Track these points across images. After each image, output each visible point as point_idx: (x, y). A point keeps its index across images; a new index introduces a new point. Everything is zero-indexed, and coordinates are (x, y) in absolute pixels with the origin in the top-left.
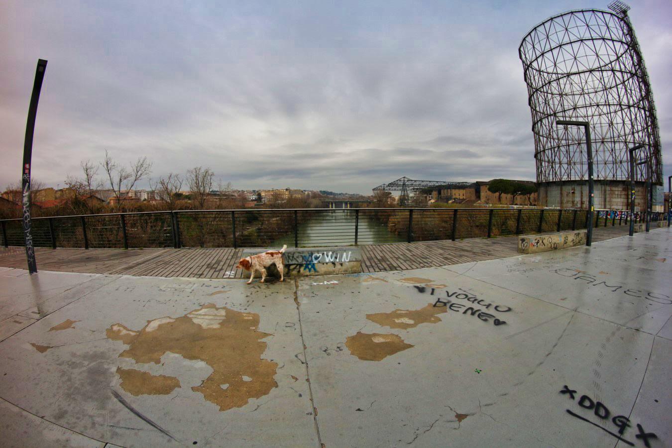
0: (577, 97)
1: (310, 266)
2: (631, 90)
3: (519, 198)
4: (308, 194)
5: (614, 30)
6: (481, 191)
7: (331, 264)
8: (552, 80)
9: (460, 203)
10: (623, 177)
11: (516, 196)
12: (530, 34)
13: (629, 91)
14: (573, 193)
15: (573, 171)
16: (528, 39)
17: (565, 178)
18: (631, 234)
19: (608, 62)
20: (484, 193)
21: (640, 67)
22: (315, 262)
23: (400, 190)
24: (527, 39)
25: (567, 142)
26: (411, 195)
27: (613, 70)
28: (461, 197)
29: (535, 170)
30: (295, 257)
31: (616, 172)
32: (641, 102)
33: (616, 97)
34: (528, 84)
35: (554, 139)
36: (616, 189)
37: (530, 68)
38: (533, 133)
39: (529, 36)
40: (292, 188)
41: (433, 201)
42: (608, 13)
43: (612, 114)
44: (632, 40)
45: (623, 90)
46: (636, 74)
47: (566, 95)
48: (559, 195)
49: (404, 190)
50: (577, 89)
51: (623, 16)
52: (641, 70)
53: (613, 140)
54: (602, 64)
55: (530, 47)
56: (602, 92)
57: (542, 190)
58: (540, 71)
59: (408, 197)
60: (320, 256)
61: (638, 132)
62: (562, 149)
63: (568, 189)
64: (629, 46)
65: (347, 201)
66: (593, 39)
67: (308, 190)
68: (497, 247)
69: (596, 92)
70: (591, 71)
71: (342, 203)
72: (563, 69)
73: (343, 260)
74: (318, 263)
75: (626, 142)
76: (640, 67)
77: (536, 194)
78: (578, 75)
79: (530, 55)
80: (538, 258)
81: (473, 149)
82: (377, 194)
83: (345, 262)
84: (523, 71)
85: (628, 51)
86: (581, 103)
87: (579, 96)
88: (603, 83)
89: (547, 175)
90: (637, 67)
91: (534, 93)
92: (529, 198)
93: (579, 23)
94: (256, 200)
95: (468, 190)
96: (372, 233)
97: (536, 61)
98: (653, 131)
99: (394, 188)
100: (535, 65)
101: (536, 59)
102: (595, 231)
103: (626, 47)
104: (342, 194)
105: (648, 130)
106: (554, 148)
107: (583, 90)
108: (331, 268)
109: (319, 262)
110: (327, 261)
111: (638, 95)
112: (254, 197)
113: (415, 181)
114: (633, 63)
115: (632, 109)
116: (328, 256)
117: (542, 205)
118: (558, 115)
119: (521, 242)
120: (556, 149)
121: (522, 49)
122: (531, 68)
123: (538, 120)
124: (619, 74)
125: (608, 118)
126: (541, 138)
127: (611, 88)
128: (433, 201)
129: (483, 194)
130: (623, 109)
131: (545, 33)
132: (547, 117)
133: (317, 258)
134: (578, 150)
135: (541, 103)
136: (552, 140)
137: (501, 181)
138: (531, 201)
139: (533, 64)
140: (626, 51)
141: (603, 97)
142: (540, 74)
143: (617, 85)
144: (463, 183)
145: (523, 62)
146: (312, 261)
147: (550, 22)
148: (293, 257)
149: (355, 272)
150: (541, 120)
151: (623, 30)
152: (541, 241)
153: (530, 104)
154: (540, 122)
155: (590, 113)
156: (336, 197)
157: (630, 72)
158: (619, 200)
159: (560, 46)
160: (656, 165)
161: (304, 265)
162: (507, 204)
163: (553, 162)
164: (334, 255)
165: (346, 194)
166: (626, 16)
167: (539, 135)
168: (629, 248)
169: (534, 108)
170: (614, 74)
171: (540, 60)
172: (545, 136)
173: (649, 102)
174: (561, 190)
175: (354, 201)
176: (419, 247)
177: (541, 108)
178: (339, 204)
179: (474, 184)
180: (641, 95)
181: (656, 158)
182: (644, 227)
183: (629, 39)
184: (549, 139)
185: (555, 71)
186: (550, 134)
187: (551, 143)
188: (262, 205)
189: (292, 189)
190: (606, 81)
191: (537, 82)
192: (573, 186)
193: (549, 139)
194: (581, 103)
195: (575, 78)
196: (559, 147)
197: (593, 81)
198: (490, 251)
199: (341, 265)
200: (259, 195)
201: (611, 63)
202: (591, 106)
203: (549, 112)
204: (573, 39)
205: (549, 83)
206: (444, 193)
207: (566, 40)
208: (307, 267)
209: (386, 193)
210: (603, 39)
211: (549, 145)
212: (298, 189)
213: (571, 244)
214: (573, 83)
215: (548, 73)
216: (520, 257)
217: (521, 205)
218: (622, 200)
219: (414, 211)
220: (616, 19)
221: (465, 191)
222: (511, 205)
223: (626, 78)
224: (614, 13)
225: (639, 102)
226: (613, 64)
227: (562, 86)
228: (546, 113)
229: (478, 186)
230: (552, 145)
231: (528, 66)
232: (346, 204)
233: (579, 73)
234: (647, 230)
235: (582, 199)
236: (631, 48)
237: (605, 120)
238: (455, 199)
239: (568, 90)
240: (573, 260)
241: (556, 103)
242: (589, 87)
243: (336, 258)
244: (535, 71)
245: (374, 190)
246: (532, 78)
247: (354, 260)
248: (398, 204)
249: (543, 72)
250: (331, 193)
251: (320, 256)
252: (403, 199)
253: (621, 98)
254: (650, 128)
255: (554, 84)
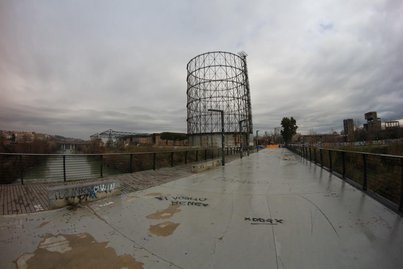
0: (212, 92)
1: (93, 195)
2: (240, 91)
3: (177, 142)
4: (48, 137)
5: (238, 64)
6: (156, 139)
7: (104, 192)
8: (201, 82)
9: (144, 146)
10: (233, 130)
11: (176, 141)
12: (195, 58)
13: (239, 91)
14: (208, 139)
15: (207, 128)
16: (194, 60)
17: (203, 132)
18: (241, 158)
19: (231, 77)
20: (158, 140)
21: (246, 81)
22: (96, 192)
23: (107, 137)
24: (193, 60)
25: (205, 113)
26: (114, 141)
27: (233, 82)
28: (144, 142)
29: (186, 127)
30: (83, 190)
31: (230, 128)
32: (244, 97)
33: (232, 93)
34: (188, 83)
35: (198, 112)
36: (230, 136)
37: (191, 75)
38: (187, 108)
39: (195, 59)
40: (37, 132)
41: (127, 145)
42: (237, 56)
43: (229, 101)
44: (245, 69)
45: (236, 91)
46: (244, 84)
47: (207, 90)
48: (200, 140)
49: (110, 137)
50: (213, 88)
51: (243, 58)
52: (247, 83)
53: (228, 114)
54: (228, 78)
55: (194, 64)
56: (226, 91)
57: (190, 138)
58: (196, 77)
59: (112, 142)
60: (98, 188)
61: (241, 110)
62: (202, 117)
63: (204, 137)
64: (243, 72)
65: (73, 143)
66: (226, 66)
67: (47, 134)
68: (178, 172)
69: (223, 90)
70: (222, 80)
71: (69, 145)
72: (208, 77)
73: (111, 189)
74: (97, 193)
75: (235, 115)
76: (246, 81)
77: (187, 140)
78: (215, 82)
79: (193, 68)
80: (203, 175)
81: (151, 115)
82: (93, 139)
83: (112, 189)
84: (187, 75)
85: (242, 74)
86: (214, 95)
87: (214, 91)
88: (227, 87)
89: (193, 131)
90: (245, 81)
91: (190, 88)
92: (183, 142)
93: (222, 57)
94: (11, 139)
95: (148, 138)
96: (90, 167)
97: (195, 72)
98: (249, 110)
99: (103, 136)
100: (194, 73)
101: (195, 71)
102: (226, 158)
103: (241, 72)
104: (69, 138)
105: (246, 110)
106: (197, 116)
107: (216, 88)
108: (105, 194)
109: (98, 192)
110: (102, 190)
111: (243, 94)
112: (9, 137)
113: (117, 132)
114: (243, 79)
115: (239, 99)
116: (102, 187)
117: (191, 146)
118: (201, 100)
119: (193, 168)
120: (199, 117)
121: (189, 65)
122: (192, 75)
123: (191, 101)
124: (235, 84)
125: (227, 103)
126: (191, 111)
127: (230, 89)
128: (127, 145)
129: (157, 141)
130: (235, 99)
131: (203, 59)
132: (196, 101)
133: (96, 189)
134: (210, 118)
135: (193, 93)
136: (197, 112)
137: (168, 133)
138: (184, 144)
139: (193, 73)
140: (241, 74)
141: (226, 93)
142: (196, 79)
143: (233, 88)
144: (145, 134)
145: (188, 71)
146: (93, 191)
147: (207, 54)
148: (82, 190)
149: (117, 195)
150: (192, 102)
151: (242, 64)
152: (202, 167)
153: (187, 93)
154: (191, 103)
155: (218, 100)
156: (66, 140)
157: (241, 83)
158: (231, 141)
159: (209, 67)
160: (250, 125)
161: (89, 195)
162: (171, 146)
163: (197, 124)
164: (106, 186)
165: (72, 138)
166: (245, 58)
167: (190, 110)
168: (241, 164)
169: (189, 95)
170: (233, 83)
171: (197, 71)
172: (193, 110)
173: (248, 97)
174: (201, 138)
175: (78, 143)
176: (139, 175)
177: (193, 95)
178: (68, 146)
179: (152, 135)
180: (245, 94)
181: (249, 121)
182: (247, 154)
183: (244, 69)
184: (195, 112)
185: (204, 78)
186: (196, 109)
187: (196, 114)
188: (16, 143)
189: (37, 133)
190: (229, 86)
191: (193, 82)
192: (207, 136)
193: (195, 112)
194: (214, 95)
195: (213, 83)
196: (200, 116)
197: (222, 85)
198: (178, 174)
199: (110, 191)
200: (13, 135)
201: (232, 78)
202: (219, 97)
203: (197, 98)
204: (217, 64)
205: (200, 84)
206: (134, 140)
207: (213, 64)
208: (91, 196)
209: (99, 139)
210: (231, 67)
211: (195, 115)
212: (41, 133)
213: (216, 166)
214: (212, 85)
215: (200, 78)
216: (195, 175)
217: (179, 146)
218: (233, 141)
219: (66, 156)
220: (240, 59)
221: (146, 138)
222: (173, 146)
223: (238, 85)
224: (240, 56)
225: (243, 97)
226: (233, 78)
227: (206, 86)
228: (195, 98)
229: (154, 136)
230: (197, 115)
231: (190, 74)
232: (72, 145)
233: (216, 81)
234: (248, 155)
235: (212, 142)
236: (243, 73)
237: (225, 104)
238: (140, 143)
239: (208, 88)
240: (217, 174)
241: (201, 94)
242: (220, 87)
243: (107, 188)
244: (193, 77)
245: (91, 136)
246: (191, 80)
247: (117, 188)
248: (106, 146)
249: (197, 78)
250: (62, 138)
251: (98, 188)
252: (109, 143)
253: (235, 94)
254: (247, 108)
255: (202, 85)
